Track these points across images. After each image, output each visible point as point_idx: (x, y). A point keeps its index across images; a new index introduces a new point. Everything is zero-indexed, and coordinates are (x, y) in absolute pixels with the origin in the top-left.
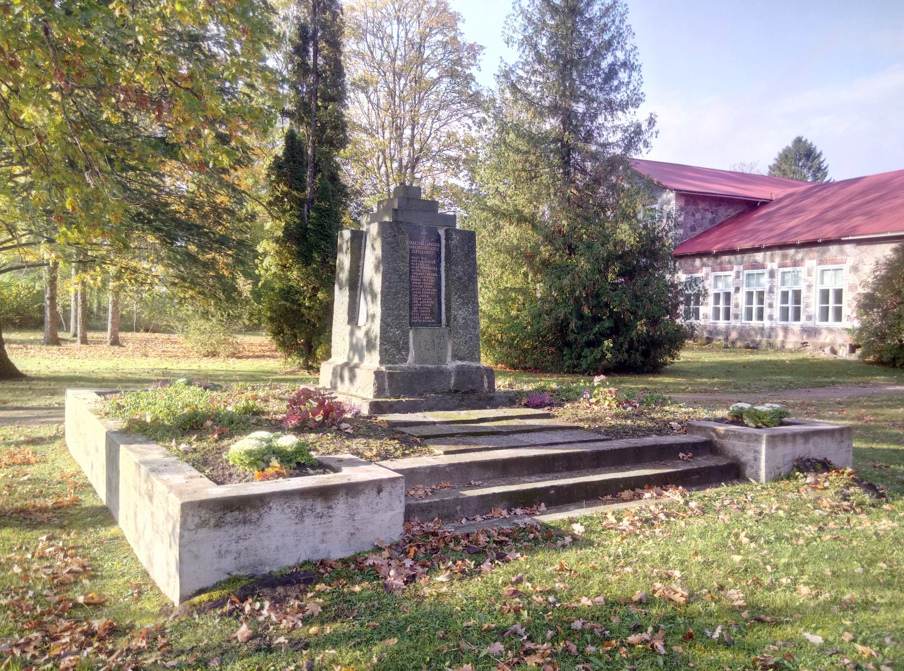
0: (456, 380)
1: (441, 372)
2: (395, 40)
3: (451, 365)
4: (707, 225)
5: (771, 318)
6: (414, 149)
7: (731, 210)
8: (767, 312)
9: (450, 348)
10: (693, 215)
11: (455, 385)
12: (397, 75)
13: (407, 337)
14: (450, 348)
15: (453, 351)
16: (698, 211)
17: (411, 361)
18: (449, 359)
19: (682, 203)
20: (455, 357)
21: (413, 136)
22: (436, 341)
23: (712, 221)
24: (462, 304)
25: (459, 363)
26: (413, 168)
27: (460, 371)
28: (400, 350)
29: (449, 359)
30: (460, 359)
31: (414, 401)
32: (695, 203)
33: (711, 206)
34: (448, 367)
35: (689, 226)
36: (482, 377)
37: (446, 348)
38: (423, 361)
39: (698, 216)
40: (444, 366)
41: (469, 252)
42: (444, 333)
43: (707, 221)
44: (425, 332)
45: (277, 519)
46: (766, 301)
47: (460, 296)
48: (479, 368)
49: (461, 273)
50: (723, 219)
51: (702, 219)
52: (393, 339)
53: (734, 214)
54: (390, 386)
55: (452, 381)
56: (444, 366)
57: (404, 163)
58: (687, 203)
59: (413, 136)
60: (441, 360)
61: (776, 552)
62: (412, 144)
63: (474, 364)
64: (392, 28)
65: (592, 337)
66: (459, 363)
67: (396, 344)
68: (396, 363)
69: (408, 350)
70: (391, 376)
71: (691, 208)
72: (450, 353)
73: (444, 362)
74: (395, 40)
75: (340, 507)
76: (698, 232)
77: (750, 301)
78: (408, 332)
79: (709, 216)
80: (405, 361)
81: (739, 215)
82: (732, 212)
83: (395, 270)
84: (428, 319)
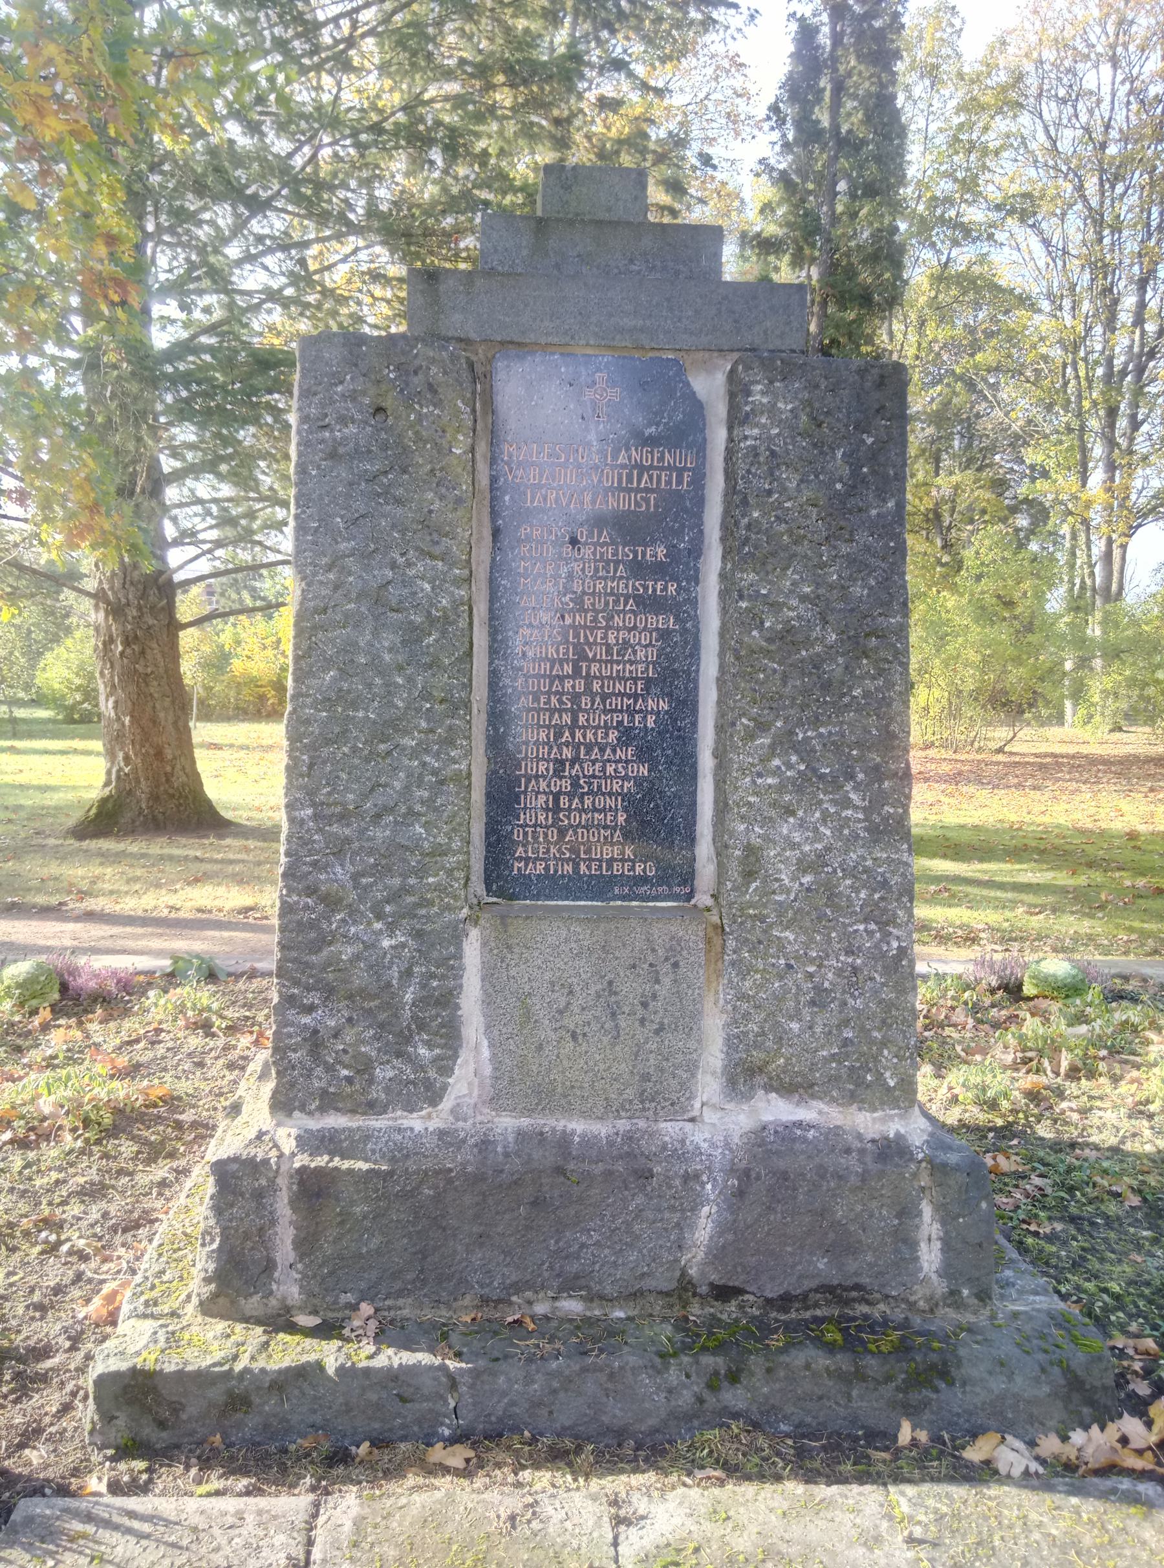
0: (722, 1229)
1: (636, 1170)
2: (1105, 105)
3: (718, 1122)
6: (1143, 333)
9: (714, 1027)
11: (717, 1255)
12: (1112, 175)
13: (452, 967)
14: (714, 1027)
15: (731, 1043)
17: (467, 1099)
18: (709, 1086)
20: (744, 1076)
21: (1142, 305)
22: (630, 989)
24: (801, 785)
25: (778, 1110)
26: (1140, 370)
27: (770, 1173)
28: (406, 1038)
29: (709, 1086)
30: (793, 1087)
31: (393, 1376)
34: (699, 1136)
36: (907, 1213)
37: (688, 1022)
38: (544, 1097)
40: (670, 1129)
41: (856, 484)
42: (675, 948)
44: (560, 943)
47: (785, 742)
48: (891, 1151)
49: (795, 611)
52: (360, 977)
54: (305, 1245)
55: (704, 1229)
56: (670, 1129)
57: (1118, 363)
59: (1142, 305)
60: (662, 1092)
62: (1139, 321)
63: (868, 1123)
64: (1098, 78)
66: (778, 1110)
67: (374, 1004)
68: (372, 1107)
69: (450, 1037)
70: (313, 1189)
72: (714, 1056)
73: (678, 1108)
74: (1105, 105)
78: (457, 937)
80: (434, 1096)
83: (377, 599)
84: (613, 852)
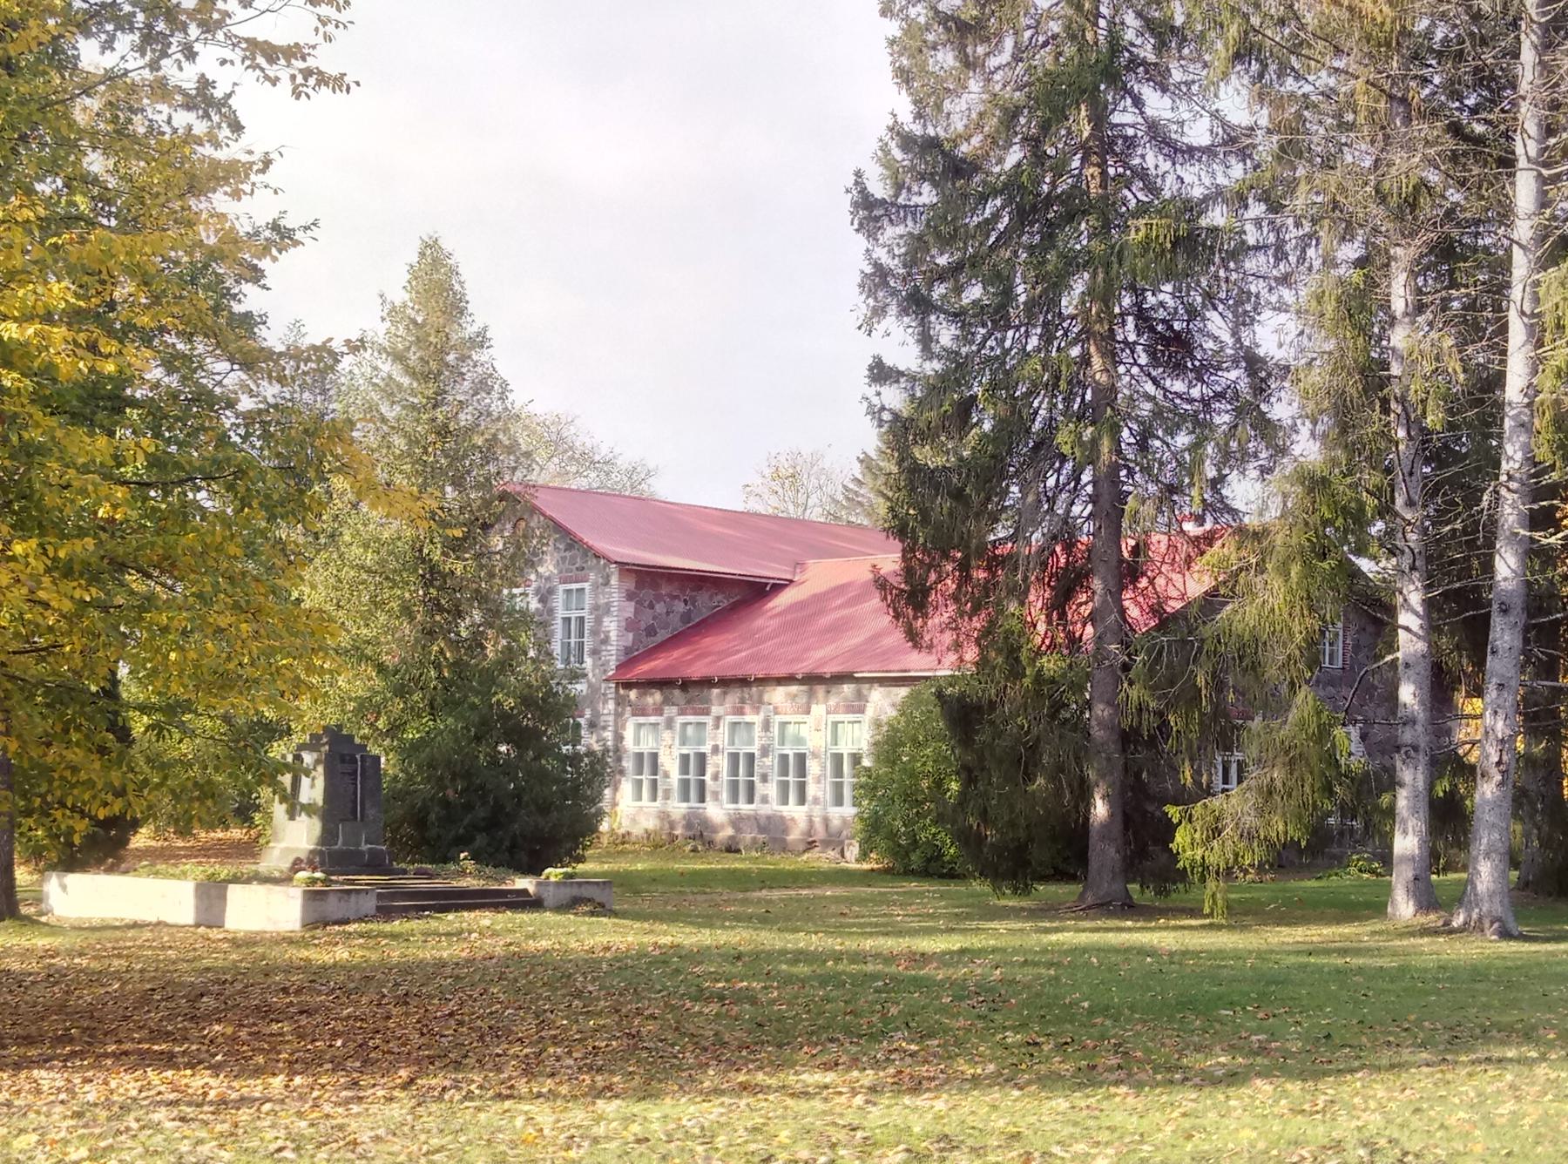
4: (676, 624)
5: (765, 800)
7: (720, 597)
8: (760, 789)
10: (652, 606)
16: (659, 598)
17: (339, 845)
19: (630, 584)
23: (686, 617)
32: (655, 585)
33: (683, 590)
35: (643, 625)
39: (660, 608)
43: (677, 618)
45: (332, 899)
46: (710, 771)
50: (706, 613)
51: (668, 613)
53: (725, 603)
58: (640, 584)
61: (306, 431)
65: (461, 831)
71: (647, 594)
75: (353, 897)
76: (659, 638)
77: (734, 770)
79: (680, 607)
81: (734, 608)
82: (720, 600)
